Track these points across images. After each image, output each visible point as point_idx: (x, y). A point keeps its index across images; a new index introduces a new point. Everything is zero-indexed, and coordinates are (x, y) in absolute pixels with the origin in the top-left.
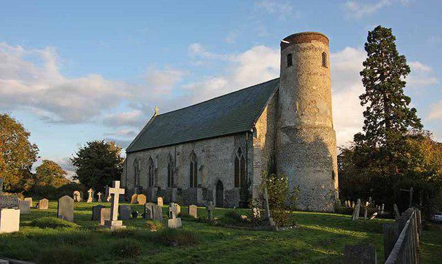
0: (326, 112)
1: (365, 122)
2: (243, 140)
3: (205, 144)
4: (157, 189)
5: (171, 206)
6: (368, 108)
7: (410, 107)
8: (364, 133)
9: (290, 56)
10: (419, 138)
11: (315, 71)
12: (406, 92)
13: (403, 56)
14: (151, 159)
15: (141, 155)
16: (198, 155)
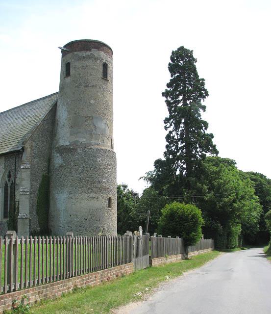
1: (167, 147)
7: (208, 132)
10: (218, 162)
11: (94, 83)
12: (204, 116)
13: (203, 80)
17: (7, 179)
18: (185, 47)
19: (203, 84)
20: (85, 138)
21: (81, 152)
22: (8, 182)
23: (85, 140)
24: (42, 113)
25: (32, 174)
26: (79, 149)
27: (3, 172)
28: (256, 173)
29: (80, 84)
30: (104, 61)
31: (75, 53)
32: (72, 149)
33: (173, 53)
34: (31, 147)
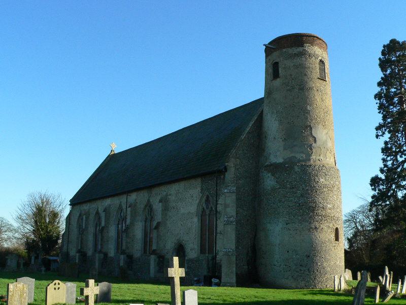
4: (102, 256)
5: (87, 286)
6: (386, 143)
8: (383, 176)
14: (97, 213)
16: (154, 207)
17: (204, 206)
18: (386, 44)
22: (205, 208)
25: (237, 199)
31: (284, 50)
33: (384, 46)
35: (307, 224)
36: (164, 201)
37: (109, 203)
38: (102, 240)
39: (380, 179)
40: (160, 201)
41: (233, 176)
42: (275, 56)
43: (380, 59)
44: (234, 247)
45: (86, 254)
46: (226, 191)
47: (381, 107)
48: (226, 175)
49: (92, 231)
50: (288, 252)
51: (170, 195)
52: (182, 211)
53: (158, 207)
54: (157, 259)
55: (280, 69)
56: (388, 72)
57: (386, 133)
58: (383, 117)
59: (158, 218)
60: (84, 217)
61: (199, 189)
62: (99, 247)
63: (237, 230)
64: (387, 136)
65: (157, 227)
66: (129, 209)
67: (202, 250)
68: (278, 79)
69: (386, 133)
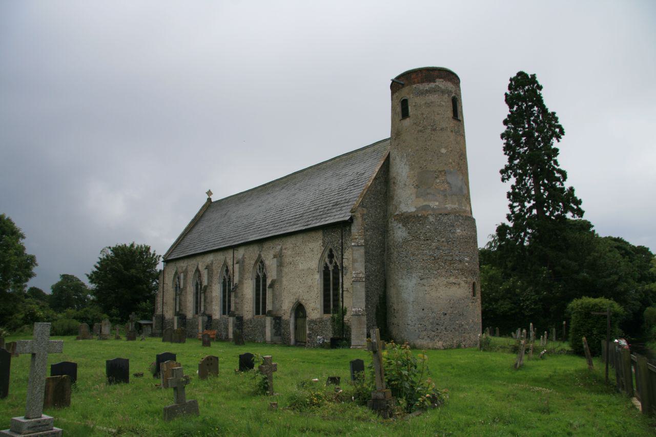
0: (461, 189)
2: (336, 236)
3: (277, 246)
4: (206, 318)
6: (513, 187)
8: (510, 224)
9: (404, 104)
13: (554, 113)
14: (198, 270)
15: (183, 264)
16: (267, 263)
17: (327, 260)
18: (512, 77)
19: (556, 119)
20: (437, 201)
21: (434, 220)
22: (328, 264)
23: (437, 204)
24: (372, 169)
25: (366, 252)
26: (430, 217)
27: (322, 250)
28: (618, 238)
29: (425, 128)
30: (453, 95)
31: (414, 86)
32: (421, 217)
33: (511, 80)
34: (363, 215)
35: (444, 279)
36: (279, 256)
37: (212, 259)
38: (205, 300)
39: (507, 227)
40: (275, 256)
41: (360, 227)
42: (404, 93)
43: (506, 94)
44: (364, 307)
45: (186, 316)
46: (353, 244)
47: (507, 148)
48: (352, 228)
49: (192, 291)
50: (423, 310)
51: (285, 249)
52: (301, 267)
53: (271, 263)
54: (274, 321)
55: (410, 107)
56: (515, 109)
57: (512, 176)
58: (509, 159)
59: (272, 275)
60: (182, 276)
61: (321, 242)
62: (202, 309)
63: (367, 288)
64: (513, 181)
65: (272, 286)
66: (237, 266)
67: (326, 310)
68: (408, 119)
69: (512, 176)
